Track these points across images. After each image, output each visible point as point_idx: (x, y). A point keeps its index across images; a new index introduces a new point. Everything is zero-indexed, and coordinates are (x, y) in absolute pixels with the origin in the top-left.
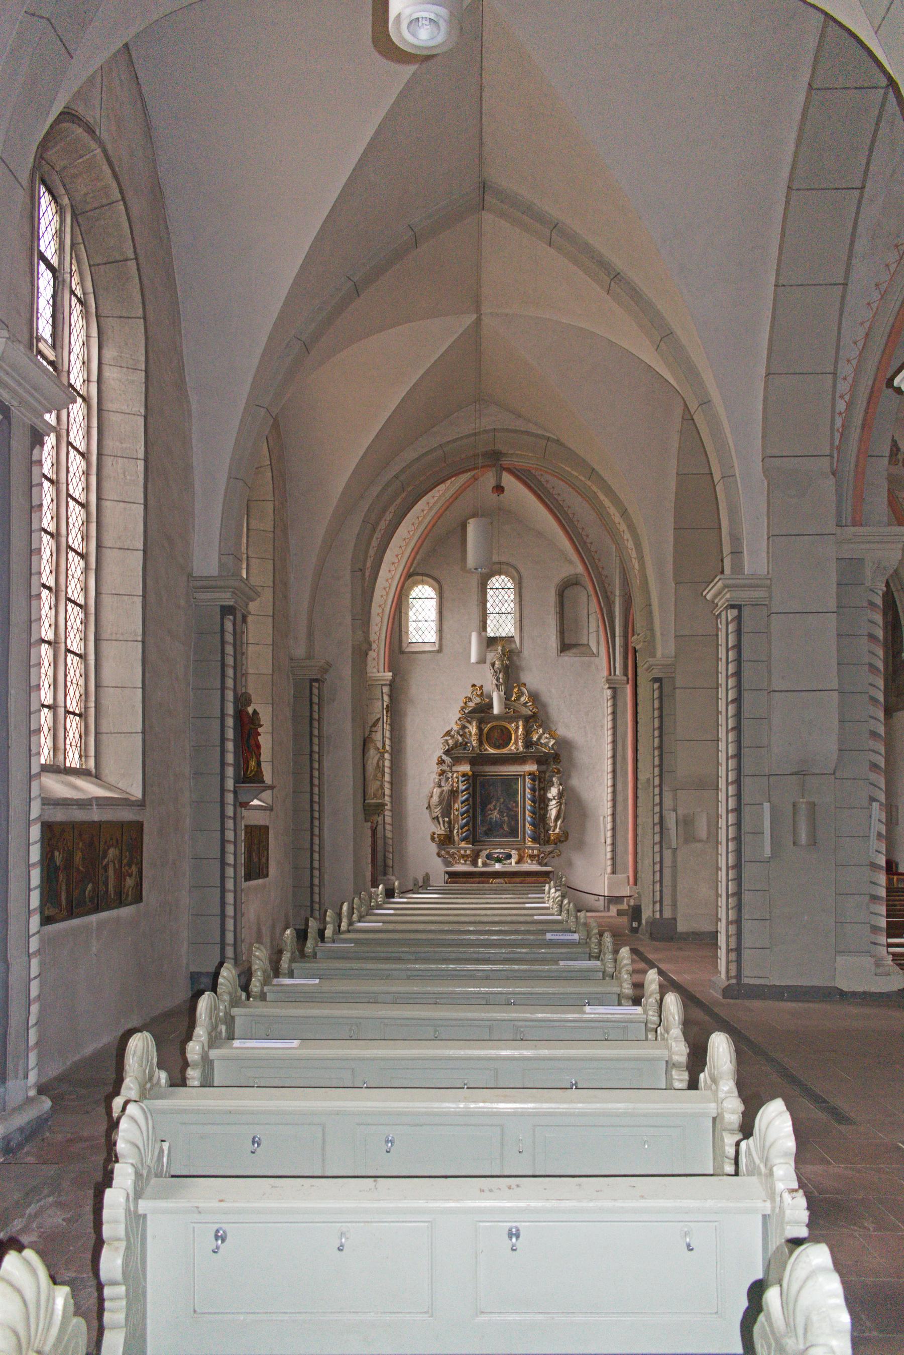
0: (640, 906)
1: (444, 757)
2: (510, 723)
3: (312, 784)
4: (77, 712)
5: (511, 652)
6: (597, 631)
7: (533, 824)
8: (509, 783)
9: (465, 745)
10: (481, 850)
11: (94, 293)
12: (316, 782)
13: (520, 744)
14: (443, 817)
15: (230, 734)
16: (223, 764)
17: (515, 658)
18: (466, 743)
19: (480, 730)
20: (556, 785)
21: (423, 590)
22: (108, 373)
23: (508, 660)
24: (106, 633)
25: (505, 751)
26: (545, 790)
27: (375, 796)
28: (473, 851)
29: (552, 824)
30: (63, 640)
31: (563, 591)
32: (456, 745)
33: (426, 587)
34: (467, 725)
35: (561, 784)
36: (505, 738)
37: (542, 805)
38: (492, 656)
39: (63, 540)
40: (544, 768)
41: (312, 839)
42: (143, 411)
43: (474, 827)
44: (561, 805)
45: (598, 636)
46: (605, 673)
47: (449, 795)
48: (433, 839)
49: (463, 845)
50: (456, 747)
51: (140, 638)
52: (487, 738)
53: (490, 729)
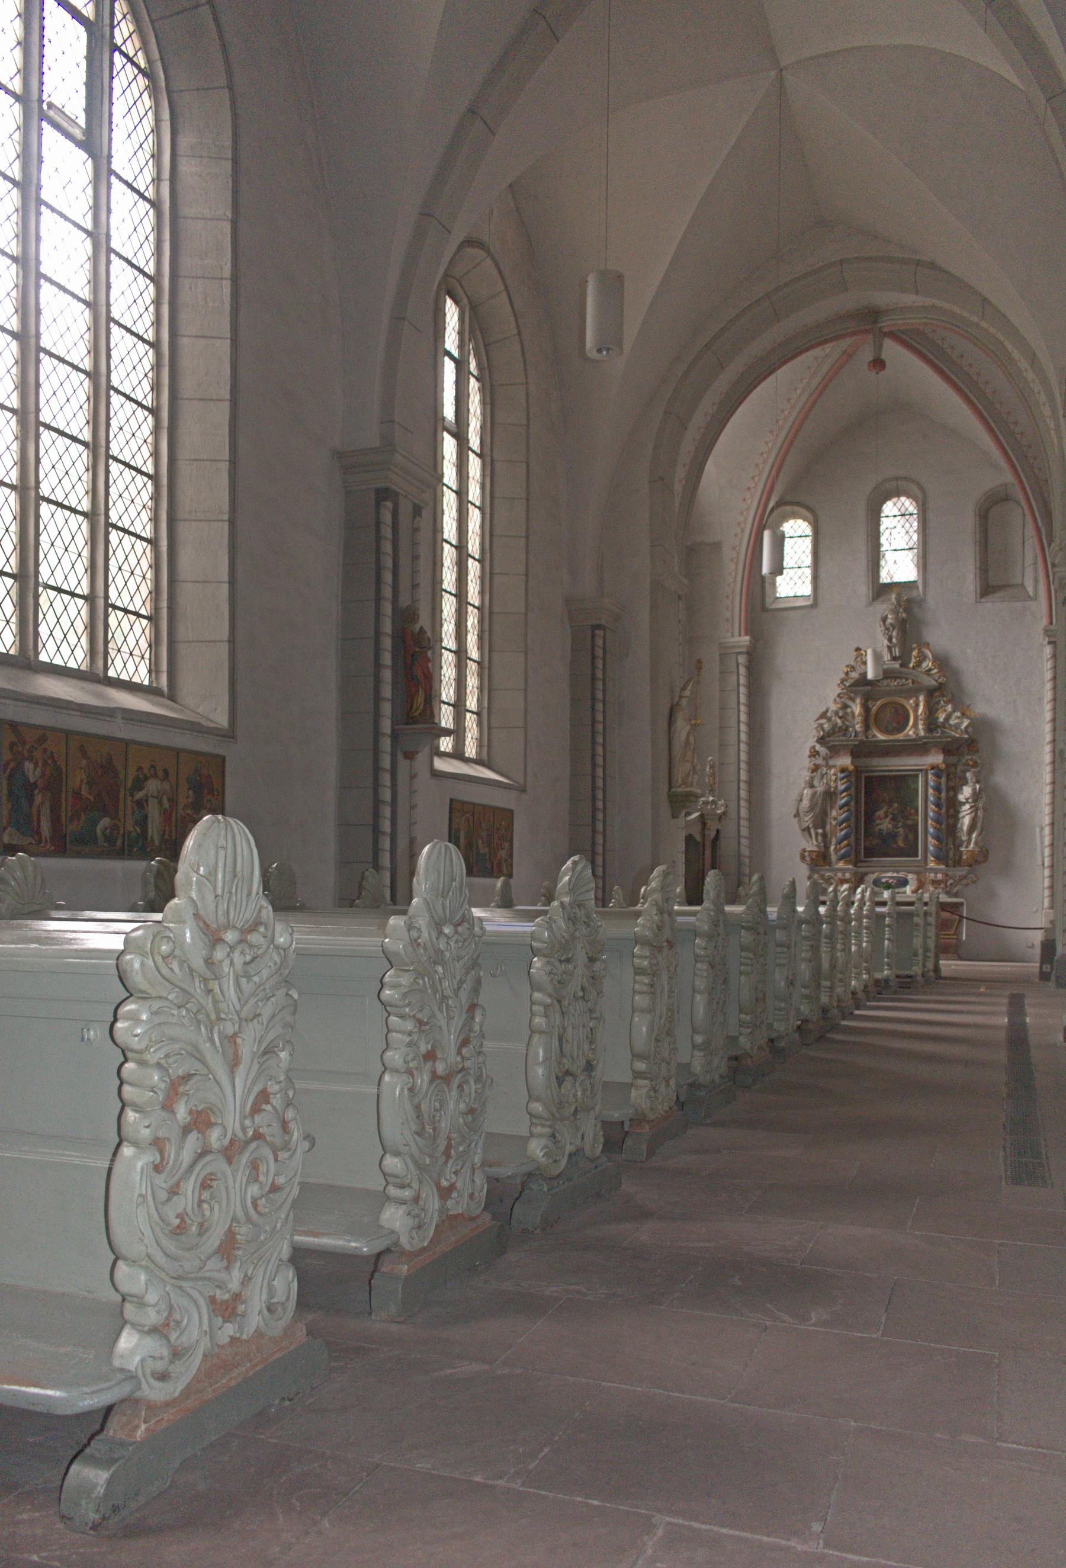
0: (1054, 940)
1: (818, 747)
2: (908, 698)
3: (594, 765)
4: (143, 612)
5: (910, 601)
6: (1035, 564)
7: (938, 838)
8: (903, 782)
9: (844, 730)
10: (866, 874)
11: (162, 59)
12: (600, 761)
13: (921, 727)
14: (816, 828)
15: (387, 659)
16: (378, 698)
17: (916, 610)
18: (847, 729)
19: (866, 709)
20: (970, 783)
21: (796, 527)
22: (186, 167)
23: (906, 610)
24: (183, 512)
25: (900, 736)
26: (955, 790)
27: (685, 783)
28: (855, 874)
29: (964, 838)
30: (103, 511)
31: (987, 511)
32: (834, 731)
33: (800, 522)
34: (850, 703)
35: (978, 782)
36: (901, 720)
37: (951, 811)
38: (884, 608)
39: (103, 380)
40: (953, 759)
41: (593, 837)
42: (229, 214)
43: (857, 840)
44: (976, 810)
45: (1036, 570)
46: (1045, 621)
47: (824, 799)
48: (803, 858)
49: (841, 865)
50: (834, 733)
51: (226, 517)
52: (875, 719)
53: (883, 706)
